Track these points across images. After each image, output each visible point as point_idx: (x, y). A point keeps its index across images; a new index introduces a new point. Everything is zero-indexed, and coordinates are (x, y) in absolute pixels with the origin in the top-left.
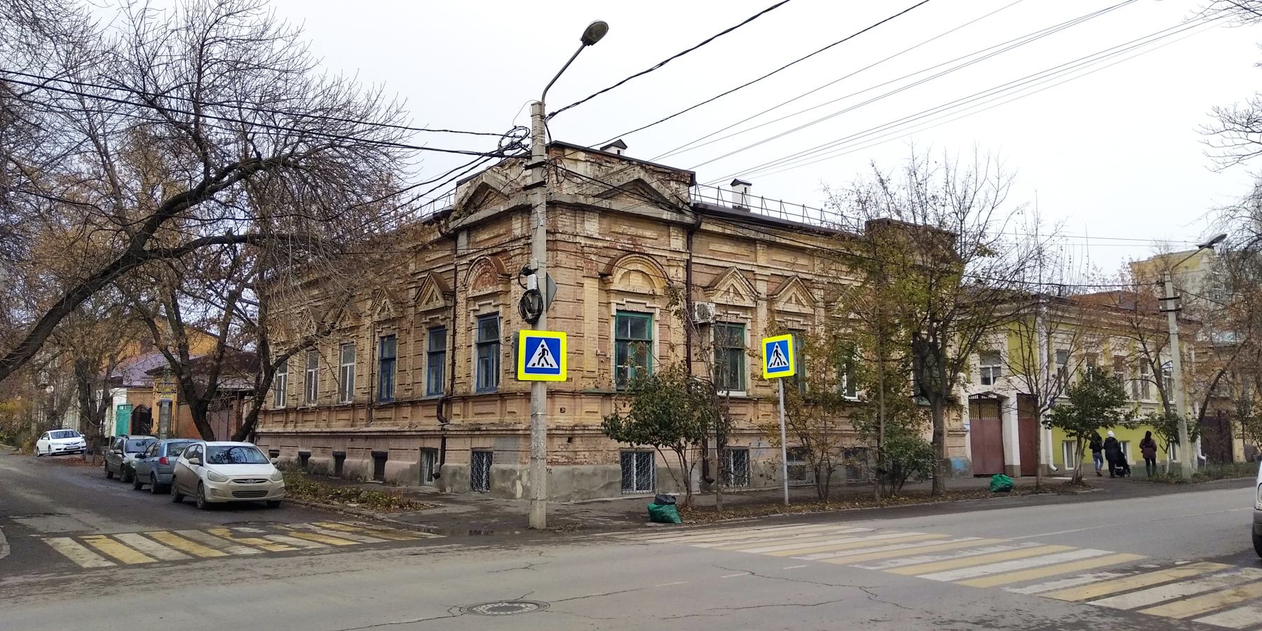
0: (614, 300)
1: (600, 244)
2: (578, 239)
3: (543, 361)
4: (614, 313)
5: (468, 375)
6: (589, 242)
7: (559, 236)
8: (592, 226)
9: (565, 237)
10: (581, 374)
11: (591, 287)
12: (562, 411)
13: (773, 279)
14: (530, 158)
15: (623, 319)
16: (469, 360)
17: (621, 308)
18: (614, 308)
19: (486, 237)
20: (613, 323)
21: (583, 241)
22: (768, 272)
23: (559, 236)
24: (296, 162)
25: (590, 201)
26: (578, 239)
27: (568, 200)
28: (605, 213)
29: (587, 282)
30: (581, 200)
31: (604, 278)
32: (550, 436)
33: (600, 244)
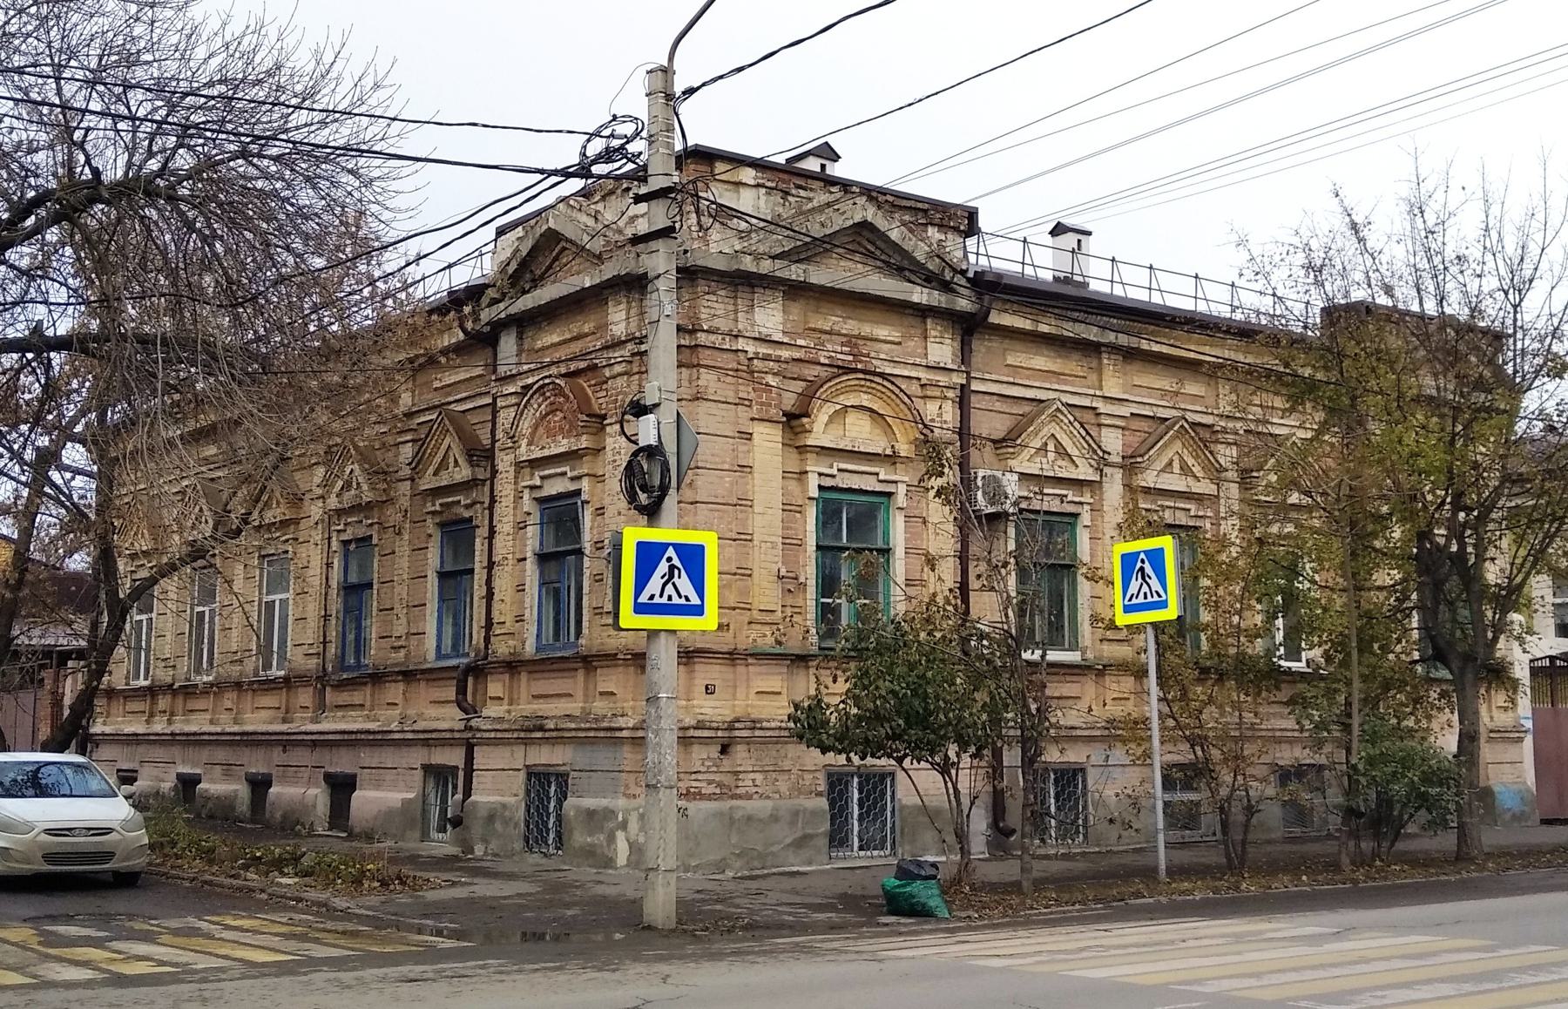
0: (814, 466)
1: (785, 354)
2: (741, 344)
3: (669, 589)
4: (814, 493)
5: (520, 619)
6: (764, 350)
7: (702, 338)
8: (770, 317)
10: (746, 617)
12: (709, 690)
15: (831, 504)
16: (520, 588)
17: (828, 482)
20: (811, 513)
21: (751, 348)
22: (1125, 411)
25: (766, 267)
26: (741, 344)
27: (721, 265)
29: (759, 430)
30: (748, 264)
33: (785, 354)
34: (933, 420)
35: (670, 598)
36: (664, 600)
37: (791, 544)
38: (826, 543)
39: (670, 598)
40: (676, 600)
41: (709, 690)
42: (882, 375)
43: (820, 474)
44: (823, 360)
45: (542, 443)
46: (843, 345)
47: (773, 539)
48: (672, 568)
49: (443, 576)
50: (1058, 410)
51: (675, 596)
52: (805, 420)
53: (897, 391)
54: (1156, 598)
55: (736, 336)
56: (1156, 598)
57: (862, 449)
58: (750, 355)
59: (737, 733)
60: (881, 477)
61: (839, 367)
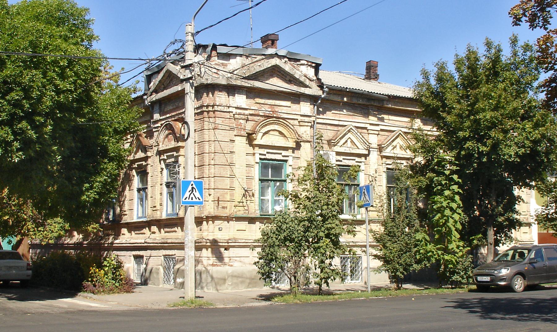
0: (258, 151)
1: (247, 112)
2: (231, 109)
3: (192, 195)
4: (258, 161)
5: (161, 205)
6: (239, 111)
7: (216, 108)
8: (240, 100)
9: (219, 108)
10: (234, 204)
11: (242, 142)
12: (220, 229)
13: (381, 133)
14: (184, 61)
15: (265, 165)
16: (161, 194)
17: (263, 157)
18: (257, 157)
19: (171, 108)
20: (257, 167)
21: (235, 111)
22: (378, 128)
23: (216, 108)
24: (15, 80)
25: (239, 83)
26: (231, 109)
27: (224, 82)
28: (252, 93)
29: (237, 139)
30: (234, 83)
31: (250, 138)
32: (198, 248)
33: (247, 112)
34: (303, 134)
35: (192, 199)
36: (190, 200)
37: (249, 178)
38: (263, 178)
39: (192, 199)
40: (194, 200)
41: (220, 229)
42: (284, 119)
43: (260, 154)
44: (261, 114)
45: (167, 144)
46: (269, 108)
47: (242, 177)
48: (193, 188)
49: (139, 190)
50: (351, 129)
51: (194, 198)
52: (254, 135)
53: (288, 124)
54: (198, 200)
55: (229, 107)
56: (198, 200)
57: (276, 145)
58: (234, 113)
59: (230, 244)
60: (283, 154)
61: (267, 116)
